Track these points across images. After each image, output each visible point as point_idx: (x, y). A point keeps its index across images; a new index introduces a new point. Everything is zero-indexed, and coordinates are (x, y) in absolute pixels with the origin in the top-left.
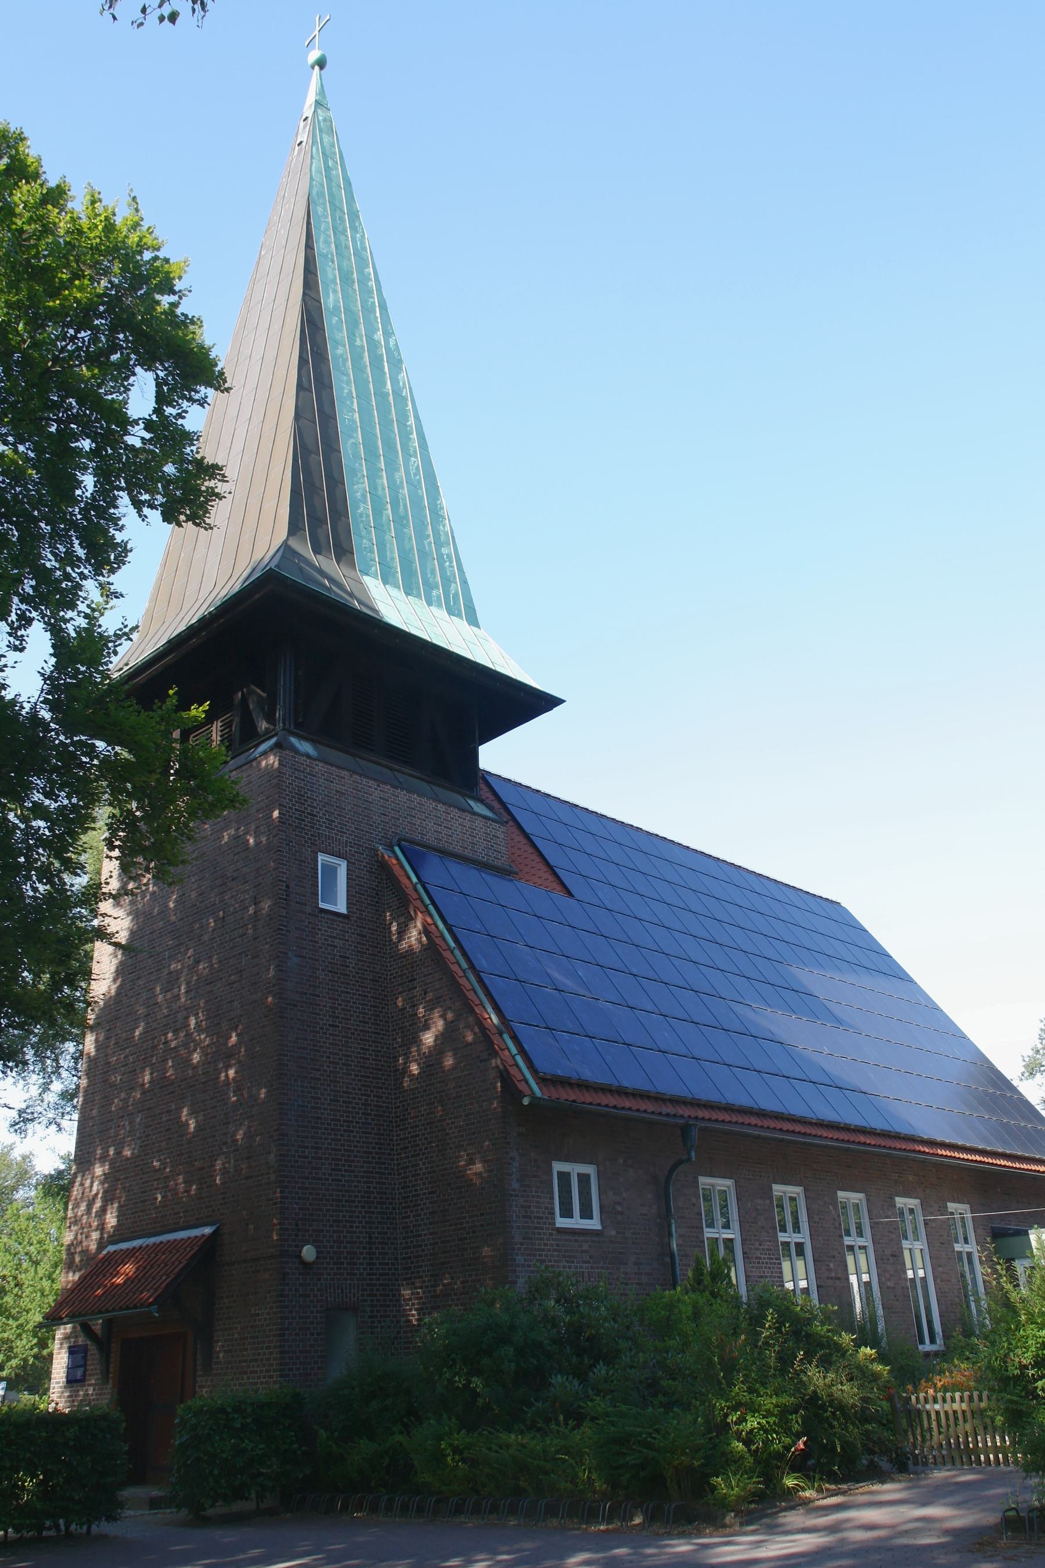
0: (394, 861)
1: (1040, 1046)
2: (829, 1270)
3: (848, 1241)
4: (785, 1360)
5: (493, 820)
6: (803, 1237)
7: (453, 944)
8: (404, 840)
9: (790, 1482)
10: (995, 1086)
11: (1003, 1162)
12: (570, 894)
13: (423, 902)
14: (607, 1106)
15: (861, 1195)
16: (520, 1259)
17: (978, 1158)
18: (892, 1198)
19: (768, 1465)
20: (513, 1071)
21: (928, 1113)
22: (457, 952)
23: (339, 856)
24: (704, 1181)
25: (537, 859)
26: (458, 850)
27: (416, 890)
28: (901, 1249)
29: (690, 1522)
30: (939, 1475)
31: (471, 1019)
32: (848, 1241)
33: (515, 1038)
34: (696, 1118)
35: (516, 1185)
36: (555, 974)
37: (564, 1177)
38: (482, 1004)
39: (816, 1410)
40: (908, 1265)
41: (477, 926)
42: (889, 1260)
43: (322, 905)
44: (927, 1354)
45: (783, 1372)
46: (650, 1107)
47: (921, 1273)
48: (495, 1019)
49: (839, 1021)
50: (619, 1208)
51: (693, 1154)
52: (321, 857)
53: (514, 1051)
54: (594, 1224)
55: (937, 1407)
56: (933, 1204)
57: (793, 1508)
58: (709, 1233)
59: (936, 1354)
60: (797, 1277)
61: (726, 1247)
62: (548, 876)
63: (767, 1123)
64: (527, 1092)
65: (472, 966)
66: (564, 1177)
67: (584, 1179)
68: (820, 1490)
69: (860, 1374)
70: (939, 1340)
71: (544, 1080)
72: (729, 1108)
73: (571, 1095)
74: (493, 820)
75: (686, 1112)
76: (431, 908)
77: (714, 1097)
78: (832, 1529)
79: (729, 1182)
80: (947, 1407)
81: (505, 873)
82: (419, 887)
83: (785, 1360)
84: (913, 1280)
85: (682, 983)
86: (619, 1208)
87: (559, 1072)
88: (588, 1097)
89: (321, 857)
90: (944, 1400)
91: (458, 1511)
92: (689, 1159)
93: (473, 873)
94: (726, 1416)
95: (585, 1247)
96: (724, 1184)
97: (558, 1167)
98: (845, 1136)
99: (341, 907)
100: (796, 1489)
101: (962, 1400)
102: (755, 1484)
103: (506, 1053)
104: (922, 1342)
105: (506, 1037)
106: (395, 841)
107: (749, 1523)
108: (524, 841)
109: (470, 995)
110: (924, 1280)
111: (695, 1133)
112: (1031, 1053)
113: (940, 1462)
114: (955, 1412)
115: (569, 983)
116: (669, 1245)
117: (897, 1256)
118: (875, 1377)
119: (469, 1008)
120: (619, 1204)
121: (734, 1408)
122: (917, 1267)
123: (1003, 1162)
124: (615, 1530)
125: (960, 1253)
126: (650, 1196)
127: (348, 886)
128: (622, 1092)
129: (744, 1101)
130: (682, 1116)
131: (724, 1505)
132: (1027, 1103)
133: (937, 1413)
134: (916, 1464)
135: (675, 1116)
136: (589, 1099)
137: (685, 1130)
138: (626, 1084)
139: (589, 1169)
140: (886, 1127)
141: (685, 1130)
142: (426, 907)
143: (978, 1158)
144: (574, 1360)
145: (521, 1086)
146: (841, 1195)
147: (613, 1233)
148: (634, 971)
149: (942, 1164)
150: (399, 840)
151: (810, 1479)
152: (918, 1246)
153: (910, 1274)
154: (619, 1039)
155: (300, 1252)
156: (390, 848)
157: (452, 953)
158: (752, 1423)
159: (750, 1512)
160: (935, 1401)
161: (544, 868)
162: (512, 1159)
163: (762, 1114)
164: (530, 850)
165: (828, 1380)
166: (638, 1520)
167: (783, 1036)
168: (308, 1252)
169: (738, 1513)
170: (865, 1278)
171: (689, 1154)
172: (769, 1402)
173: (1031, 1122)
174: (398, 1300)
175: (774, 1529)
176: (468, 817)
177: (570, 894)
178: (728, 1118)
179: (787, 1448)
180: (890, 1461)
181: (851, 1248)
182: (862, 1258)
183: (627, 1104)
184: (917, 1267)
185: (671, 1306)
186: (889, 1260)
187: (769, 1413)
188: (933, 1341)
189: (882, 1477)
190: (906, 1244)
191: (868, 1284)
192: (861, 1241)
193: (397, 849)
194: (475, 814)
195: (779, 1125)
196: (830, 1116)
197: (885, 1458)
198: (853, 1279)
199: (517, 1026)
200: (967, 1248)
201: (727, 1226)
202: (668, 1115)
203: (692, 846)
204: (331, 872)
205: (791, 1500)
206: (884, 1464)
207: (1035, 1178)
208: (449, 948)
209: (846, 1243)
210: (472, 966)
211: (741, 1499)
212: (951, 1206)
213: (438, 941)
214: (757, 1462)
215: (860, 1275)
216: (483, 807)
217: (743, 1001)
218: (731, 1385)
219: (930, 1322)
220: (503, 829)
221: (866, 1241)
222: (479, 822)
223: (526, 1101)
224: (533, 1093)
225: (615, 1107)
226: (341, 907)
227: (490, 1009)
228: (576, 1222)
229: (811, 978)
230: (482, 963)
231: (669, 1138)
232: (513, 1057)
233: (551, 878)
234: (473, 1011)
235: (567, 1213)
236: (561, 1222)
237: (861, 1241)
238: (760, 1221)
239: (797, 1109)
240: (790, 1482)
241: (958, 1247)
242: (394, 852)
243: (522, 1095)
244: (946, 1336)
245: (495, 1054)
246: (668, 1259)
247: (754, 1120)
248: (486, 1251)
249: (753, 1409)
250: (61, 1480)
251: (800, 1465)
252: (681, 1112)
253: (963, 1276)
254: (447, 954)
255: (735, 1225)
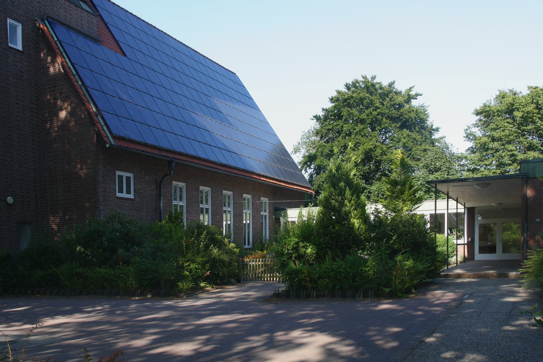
0: (46, 28)
1: (300, 142)
2: (217, 218)
3: (224, 209)
4: (207, 247)
5: (91, 14)
6: (209, 206)
7: (75, 73)
8: (50, 18)
9: (202, 285)
10: (284, 155)
11: (283, 184)
12: (125, 55)
13: (60, 50)
14: (140, 150)
15: (231, 193)
16: (102, 208)
17: (275, 182)
18: (242, 195)
19: (197, 279)
20: (102, 132)
21: (256, 162)
22: (77, 77)
23: (18, 21)
24: (174, 183)
25: (110, 36)
26: (75, 26)
27: (56, 44)
28: (243, 213)
29: (168, 296)
30: (251, 284)
31: (83, 108)
32: (224, 209)
33: (103, 118)
34: (174, 158)
35: (101, 179)
36: (119, 92)
37: (120, 177)
38: (88, 102)
39: (214, 263)
40: (244, 219)
41: (85, 66)
42: (238, 216)
43: (10, 45)
44: (246, 249)
45: (206, 251)
46: (157, 152)
47: (248, 222)
48: (94, 109)
49: (230, 124)
50: (141, 191)
51: (172, 172)
52: (9, 21)
53: (103, 124)
54: (131, 196)
55: (253, 263)
56: (256, 197)
57: (203, 292)
58: (174, 203)
59: (250, 249)
60: (206, 219)
61: (180, 208)
62: (115, 44)
63: (201, 162)
64: (108, 141)
65: (83, 84)
66: (120, 177)
67: (128, 179)
68: (213, 287)
69: (230, 252)
70: (251, 244)
71: (115, 137)
72: (187, 156)
73: (126, 145)
74: (91, 14)
75: (171, 155)
76: (64, 53)
77: (181, 150)
78: (218, 297)
79: (184, 184)
80: (257, 263)
81: (96, 41)
82: (58, 42)
83: (207, 247)
84: (245, 224)
85: (171, 102)
86: (141, 191)
87: (121, 135)
88: (133, 146)
89: (9, 21)
90: (256, 261)
91: (80, 294)
92: (171, 174)
93: (81, 38)
94: (183, 264)
95: (127, 204)
96: (182, 184)
97: (118, 173)
98: (229, 170)
99: (19, 47)
100: (205, 287)
101: (262, 261)
102: (191, 285)
103: (99, 124)
104: (245, 245)
105: (99, 117)
106: (45, 17)
107: (189, 296)
108: (104, 26)
109: (83, 97)
110: (249, 224)
111: (174, 164)
112: (297, 144)
113: (252, 280)
114: (259, 265)
115: (124, 96)
116: (160, 206)
117: (241, 215)
118: (235, 253)
119: (82, 103)
120: (142, 189)
121: (187, 261)
122: (247, 220)
123: (283, 184)
124: (142, 299)
125: (262, 215)
126: (153, 187)
127: (22, 37)
128: (146, 145)
129: (193, 153)
130: (169, 157)
131: (181, 291)
132: (294, 163)
133: (253, 265)
134: (243, 281)
135: (166, 157)
136: (133, 147)
137: (170, 162)
138: (148, 142)
139: (131, 175)
140: (244, 168)
141: (170, 162)
142: (62, 53)
143: (275, 182)
144: (125, 244)
145: (106, 139)
146: (225, 192)
147: (139, 200)
148: (152, 94)
149: (262, 183)
150: (47, 17)
151: (210, 284)
152: (248, 212)
153: (244, 222)
154: (145, 123)
155: (6, 199)
156: (43, 20)
157: (74, 76)
158: (193, 266)
159: (190, 293)
160: (253, 261)
161: (113, 41)
162: (100, 168)
163: (199, 159)
164: (107, 31)
165: (220, 253)
166: (149, 296)
167: (209, 128)
168: (10, 200)
169: (186, 294)
170: (229, 222)
171: (171, 172)
172: (199, 259)
173: (294, 170)
174: (48, 221)
175: (199, 299)
176: (80, 10)
177: (125, 55)
178: (186, 159)
179: (203, 275)
180: (235, 279)
181: (225, 211)
182: (229, 216)
183: (148, 151)
184: (247, 220)
185: (161, 228)
186: (238, 216)
187: (199, 263)
188: (248, 245)
189: (232, 284)
190: (244, 211)
191: (229, 225)
192: (229, 209)
193: (46, 22)
194: (83, 9)
195: (205, 164)
196: (224, 162)
197: (333, 204)
198: (224, 223)
199: (105, 115)
200: (265, 214)
201: (181, 199)
202: (163, 156)
203: (177, 39)
204: (14, 28)
205: (203, 290)
206: (233, 280)
207: (292, 190)
208: (73, 74)
209: (174, 203)
210: (83, 84)
211: (187, 290)
212: (262, 198)
213: (68, 70)
214: (193, 278)
215: (227, 220)
216: (86, 6)
217: (194, 111)
218: (187, 253)
219: (249, 238)
220: (96, 19)
221: (231, 209)
222: (85, 14)
223: (107, 146)
224: (111, 142)
225: (143, 151)
226: (19, 47)
227: (92, 105)
228: (124, 195)
229: (221, 105)
230: (88, 83)
231: (163, 166)
232: (102, 126)
233: (117, 46)
234: (85, 105)
235: (121, 191)
236: (119, 195)
237: (229, 209)
238: (194, 200)
239: (213, 158)
240: (202, 285)
241: (262, 213)
242: (45, 23)
243: (106, 143)
244: (254, 243)
245: (95, 125)
246: (158, 211)
247: (196, 161)
248: (87, 205)
249: (194, 262)
250: (464, 161)
251: (207, 279)
252: (169, 155)
253: (262, 223)
254: (72, 77)
255: (185, 200)
